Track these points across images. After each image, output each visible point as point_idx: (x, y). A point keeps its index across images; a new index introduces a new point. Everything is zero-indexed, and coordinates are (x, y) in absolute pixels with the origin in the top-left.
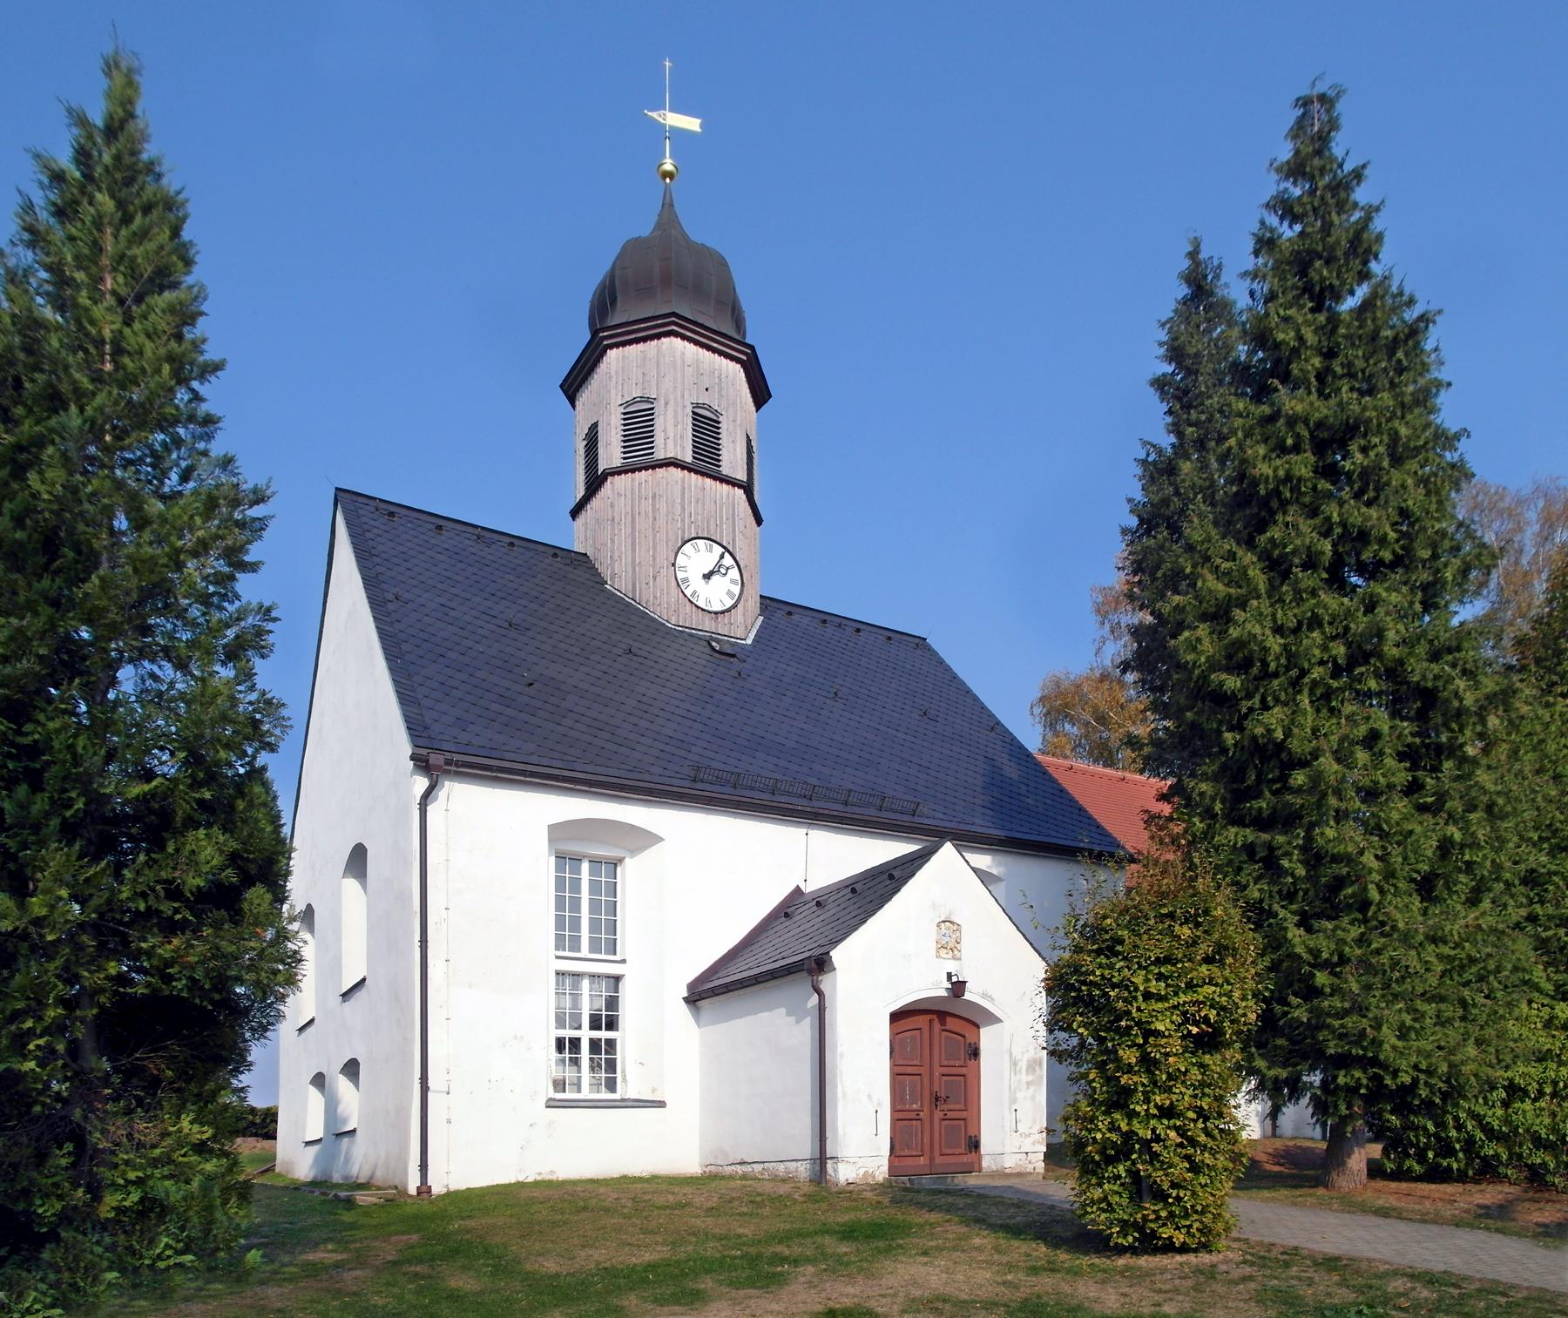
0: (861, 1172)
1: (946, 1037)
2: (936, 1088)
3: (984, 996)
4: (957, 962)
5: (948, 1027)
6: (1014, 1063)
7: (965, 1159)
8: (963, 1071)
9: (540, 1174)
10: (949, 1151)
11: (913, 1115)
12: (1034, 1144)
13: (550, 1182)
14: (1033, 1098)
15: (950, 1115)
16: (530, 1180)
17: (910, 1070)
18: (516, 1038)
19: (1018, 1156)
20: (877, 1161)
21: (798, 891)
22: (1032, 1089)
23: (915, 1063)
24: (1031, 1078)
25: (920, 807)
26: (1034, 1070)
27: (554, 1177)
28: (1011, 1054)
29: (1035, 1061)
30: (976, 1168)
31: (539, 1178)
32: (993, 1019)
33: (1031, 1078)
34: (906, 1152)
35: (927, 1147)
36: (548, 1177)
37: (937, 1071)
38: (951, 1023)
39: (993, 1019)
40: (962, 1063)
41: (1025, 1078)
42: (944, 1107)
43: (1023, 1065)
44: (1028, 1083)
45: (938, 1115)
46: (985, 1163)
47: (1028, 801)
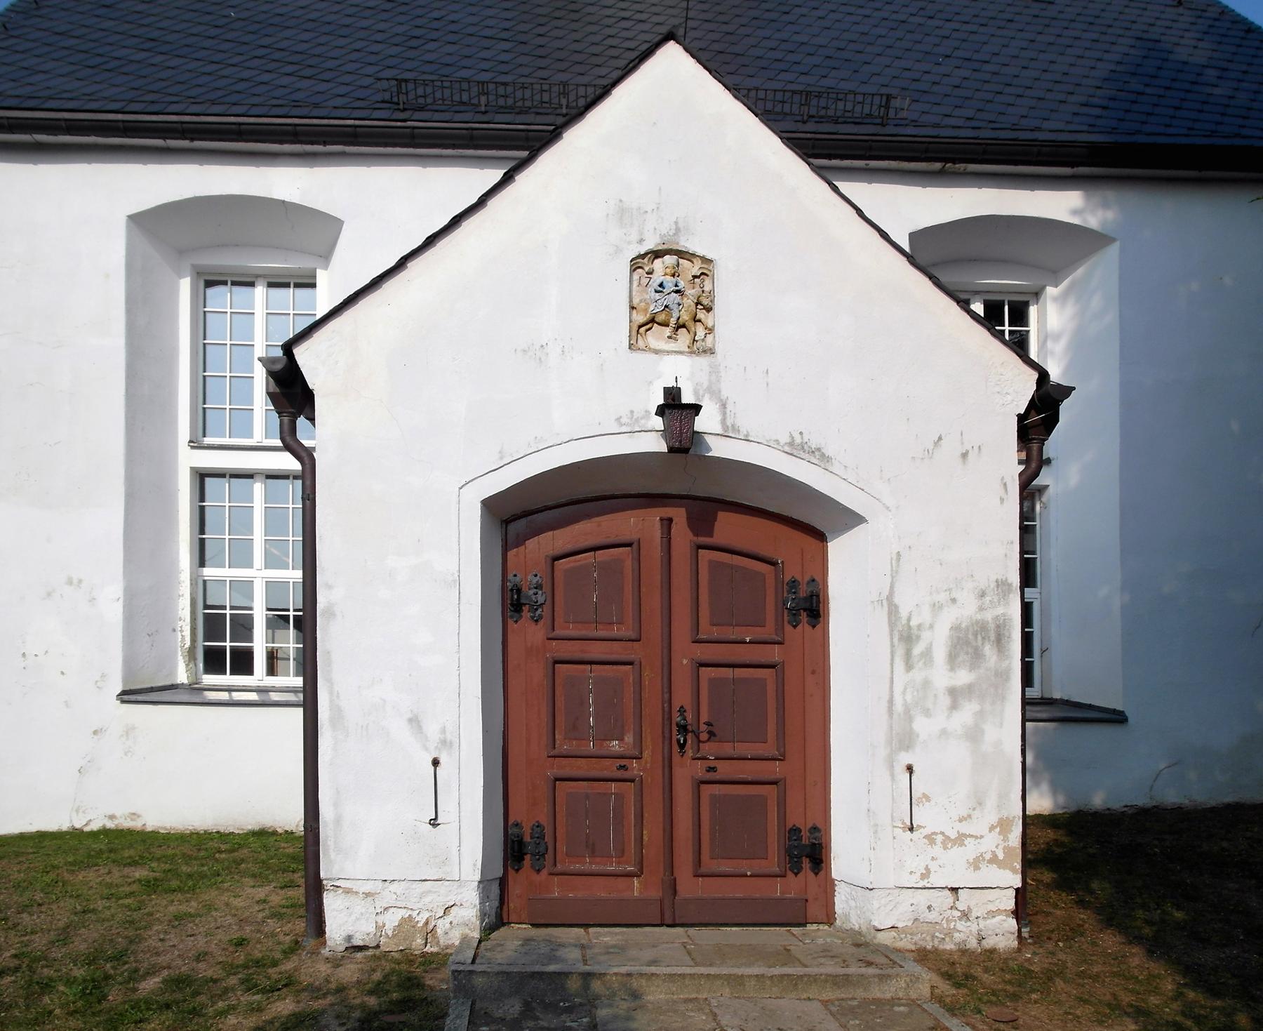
0: (391, 920)
1: (713, 566)
2: (682, 697)
3: (796, 448)
4: (703, 361)
5: (719, 537)
6: (906, 637)
7: (778, 889)
8: (774, 654)
9: (112, 817)
10: (725, 867)
11: (609, 769)
12: (976, 864)
13: (130, 833)
14: (974, 735)
15: (725, 769)
16: (94, 827)
17: (597, 651)
18: (70, 582)
19: (923, 898)
20: (438, 897)
21: (1019, 416)
22: (968, 712)
23: (615, 632)
24: (963, 677)
25: (896, 103)
26: (977, 656)
27: (136, 825)
28: (893, 610)
29: (980, 629)
30: (814, 910)
31: (110, 825)
32: (851, 519)
33: (963, 677)
34: (588, 865)
35: (653, 851)
36: (127, 824)
37: (683, 662)
38: (728, 527)
39: (851, 519)
40: (767, 632)
41: (942, 677)
42: (709, 749)
43: (938, 639)
44: (953, 693)
45: (687, 770)
46: (842, 902)
47: (1217, 91)
